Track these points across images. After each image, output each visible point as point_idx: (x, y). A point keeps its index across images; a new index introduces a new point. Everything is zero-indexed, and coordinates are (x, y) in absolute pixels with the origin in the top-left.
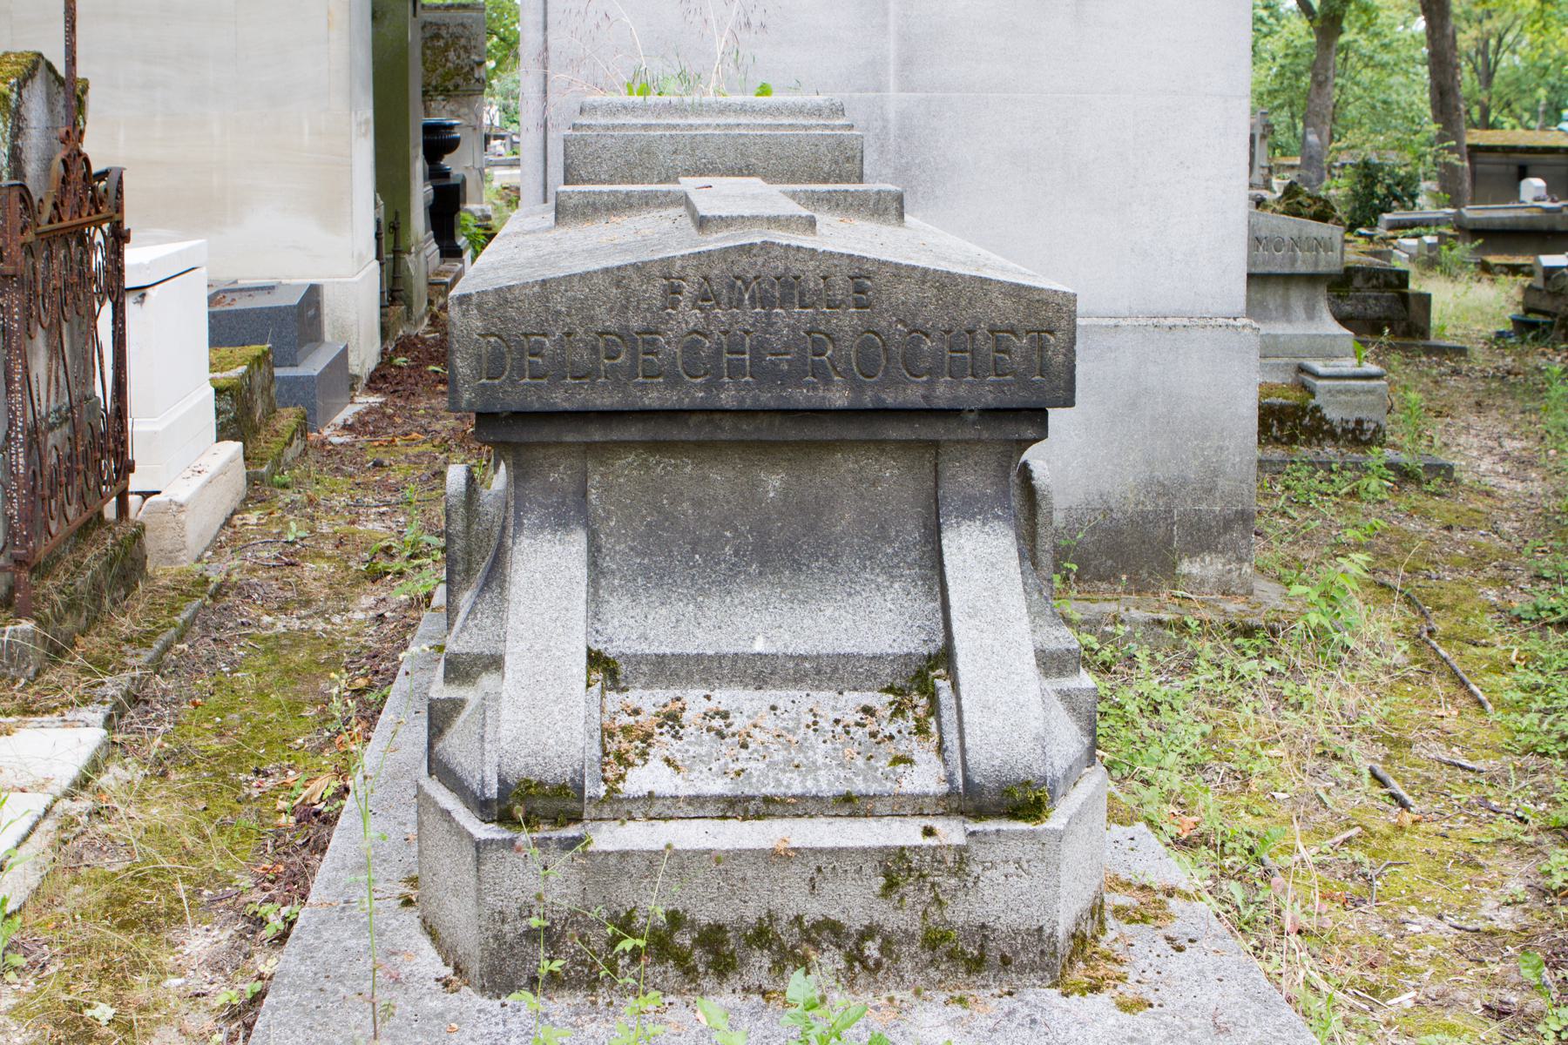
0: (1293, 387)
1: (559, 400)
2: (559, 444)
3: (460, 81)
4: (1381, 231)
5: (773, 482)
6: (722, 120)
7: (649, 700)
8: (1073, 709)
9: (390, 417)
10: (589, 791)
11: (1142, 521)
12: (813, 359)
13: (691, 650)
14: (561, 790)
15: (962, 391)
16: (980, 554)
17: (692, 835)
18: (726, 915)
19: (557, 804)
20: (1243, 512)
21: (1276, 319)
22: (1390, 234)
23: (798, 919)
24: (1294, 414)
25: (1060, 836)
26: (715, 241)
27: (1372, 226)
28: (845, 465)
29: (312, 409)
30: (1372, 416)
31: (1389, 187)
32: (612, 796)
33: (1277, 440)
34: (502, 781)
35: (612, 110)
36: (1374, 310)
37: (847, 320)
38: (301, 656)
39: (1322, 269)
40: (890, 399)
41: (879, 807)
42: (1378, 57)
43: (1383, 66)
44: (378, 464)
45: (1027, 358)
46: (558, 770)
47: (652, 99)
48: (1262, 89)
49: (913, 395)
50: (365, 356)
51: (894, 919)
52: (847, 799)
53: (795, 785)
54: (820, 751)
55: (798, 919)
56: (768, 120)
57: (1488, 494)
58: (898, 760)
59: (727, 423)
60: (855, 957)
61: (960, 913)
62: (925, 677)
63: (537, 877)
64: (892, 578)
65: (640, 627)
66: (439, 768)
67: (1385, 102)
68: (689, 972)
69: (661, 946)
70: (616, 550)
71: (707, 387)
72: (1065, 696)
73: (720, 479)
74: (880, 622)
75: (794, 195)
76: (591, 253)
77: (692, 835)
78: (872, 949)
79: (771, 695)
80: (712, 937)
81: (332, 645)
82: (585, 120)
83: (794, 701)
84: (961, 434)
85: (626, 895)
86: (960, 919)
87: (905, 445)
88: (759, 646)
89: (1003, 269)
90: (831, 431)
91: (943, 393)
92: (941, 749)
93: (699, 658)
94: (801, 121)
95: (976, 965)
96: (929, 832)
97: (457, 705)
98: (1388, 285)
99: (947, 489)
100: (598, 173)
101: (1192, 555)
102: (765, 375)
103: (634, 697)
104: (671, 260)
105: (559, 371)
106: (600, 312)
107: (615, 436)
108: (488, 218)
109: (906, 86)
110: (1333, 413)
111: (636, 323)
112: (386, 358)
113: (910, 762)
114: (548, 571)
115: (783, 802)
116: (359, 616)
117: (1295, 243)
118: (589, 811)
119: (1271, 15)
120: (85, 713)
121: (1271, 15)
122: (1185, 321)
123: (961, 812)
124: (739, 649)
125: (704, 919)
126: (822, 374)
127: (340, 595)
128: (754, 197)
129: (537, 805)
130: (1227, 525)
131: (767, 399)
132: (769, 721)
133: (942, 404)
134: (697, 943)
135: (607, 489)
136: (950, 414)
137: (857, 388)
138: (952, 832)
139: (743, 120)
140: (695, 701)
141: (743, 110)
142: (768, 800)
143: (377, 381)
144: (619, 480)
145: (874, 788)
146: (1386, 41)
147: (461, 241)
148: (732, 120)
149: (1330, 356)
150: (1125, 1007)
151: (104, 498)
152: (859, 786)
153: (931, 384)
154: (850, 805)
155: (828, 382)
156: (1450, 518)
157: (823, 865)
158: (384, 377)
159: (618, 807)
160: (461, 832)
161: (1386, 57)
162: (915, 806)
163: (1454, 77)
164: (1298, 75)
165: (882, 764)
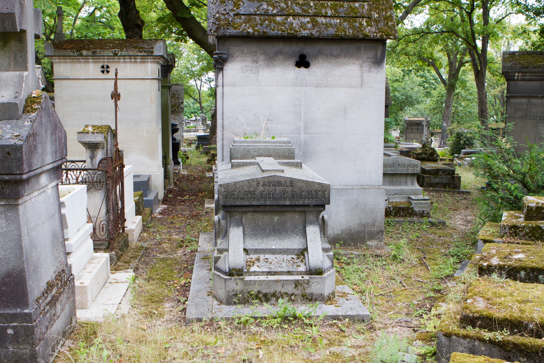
0: (407, 203)
1: (238, 203)
3: (176, 108)
4: (462, 155)
5: (276, 218)
6: (264, 145)
7: (254, 257)
9: (171, 211)
10: (244, 271)
11: (358, 232)
12: (283, 195)
13: (261, 248)
14: (239, 270)
15: (310, 202)
16: (313, 231)
17: (263, 278)
18: (268, 291)
19: (239, 272)
21: (403, 185)
22: (464, 156)
23: (280, 292)
24: (406, 209)
25: (325, 278)
26: (266, 175)
27: (460, 153)
28: (289, 215)
29: (152, 208)
30: (426, 210)
31: (465, 141)
32: (248, 272)
33: (402, 216)
34: (229, 268)
35: (241, 142)
36: (445, 181)
37: (289, 189)
38: (169, 262)
39: (415, 172)
40: (297, 203)
41: (294, 273)
42: (468, 98)
43: (469, 100)
44: (172, 223)
46: (239, 267)
47: (249, 140)
48: (431, 107)
49: (301, 202)
50: (161, 196)
52: (289, 272)
54: (284, 264)
55: (280, 292)
56: (274, 145)
57: (454, 229)
58: (297, 266)
59: (268, 207)
61: (308, 291)
62: (302, 253)
63: (235, 285)
64: (297, 235)
65: (253, 244)
66: (217, 269)
67: (469, 112)
68: (261, 301)
69: (257, 297)
70: (248, 230)
71: (264, 201)
72: (328, 256)
73: (266, 217)
74: (294, 243)
75: (279, 163)
76: (242, 176)
77: (263, 278)
78: (293, 297)
79: (275, 256)
80: (265, 295)
81: (175, 260)
82: (235, 144)
83: (280, 257)
84: (309, 209)
85: (250, 288)
86: (308, 292)
87: (300, 211)
88: (273, 247)
89: (319, 179)
90: (286, 209)
91: (306, 202)
92: (305, 264)
93: (263, 249)
94: (281, 145)
95: (311, 300)
96: (303, 277)
97: (219, 258)
98: (449, 174)
99: (307, 219)
100: (238, 156)
101: (369, 240)
102: (275, 199)
103: (251, 256)
104: (258, 178)
105: (238, 198)
107: (248, 210)
108: (186, 152)
109: (306, 133)
110: (416, 209)
111: (252, 190)
112: (166, 196)
113: (300, 266)
114: (236, 234)
115: (278, 272)
116: (179, 254)
117: (409, 165)
118: (244, 274)
119: (436, 82)
120: (129, 270)
121: (436, 82)
123: (309, 274)
124: (270, 247)
125: (264, 292)
126: (285, 199)
127: (174, 251)
128: (272, 164)
129: (235, 273)
131: (275, 203)
132: (275, 260)
133: (306, 204)
134: (263, 296)
135: (246, 219)
136: (308, 206)
138: (307, 277)
139: (269, 144)
140: (262, 257)
141: (269, 142)
142: (275, 272)
143: (165, 201)
144: (248, 218)
145: (293, 270)
146: (471, 92)
147: (180, 160)
148: (266, 144)
149: (417, 195)
150: (336, 306)
151: (119, 229)
152: (291, 270)
153: (304, 200)
154: (289, 273)
155: (286, 200)
156: (441, 234)
158: (166, 200)
159: (249, 273)
160: (222, 278)
161: (470, 97)
162: (300, 273)
163: (486, 107)
164: (442, 103)
165: (295, 267)
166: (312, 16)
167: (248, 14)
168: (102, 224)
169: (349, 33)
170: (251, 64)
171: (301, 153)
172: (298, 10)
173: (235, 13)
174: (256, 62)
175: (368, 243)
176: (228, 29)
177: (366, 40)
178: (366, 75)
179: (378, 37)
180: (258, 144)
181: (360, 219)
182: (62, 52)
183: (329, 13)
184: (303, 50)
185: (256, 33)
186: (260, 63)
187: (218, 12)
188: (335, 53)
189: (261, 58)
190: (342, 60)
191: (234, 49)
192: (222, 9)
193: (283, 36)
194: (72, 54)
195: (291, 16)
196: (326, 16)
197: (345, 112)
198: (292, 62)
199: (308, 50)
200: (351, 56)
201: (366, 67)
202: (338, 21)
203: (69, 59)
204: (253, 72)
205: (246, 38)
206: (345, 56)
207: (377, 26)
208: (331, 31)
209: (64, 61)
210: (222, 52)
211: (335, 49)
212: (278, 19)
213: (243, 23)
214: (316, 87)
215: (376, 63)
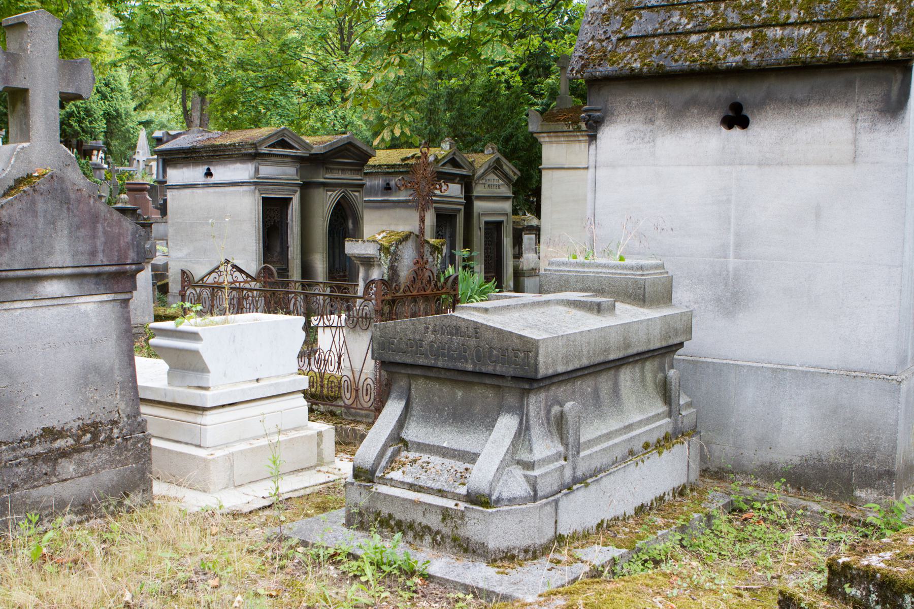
2: (485, 384)
5: (460, 393)
8: (528, 482)
11: (836, 467)
15: (504, 369)
18: (403, 518)
20: (889, 471)
23: (420, 523)
28: (479, 391)
37: (473, 342)
40: (484, 370)
45: (523, 360)
49: (489, 369)
51: (446, 530)
53: (430, 484)
55: (420, 523)
60: (434, 539)
61: (462, 532)
73: (445, 390)
88: (445, 445)
91: (499, 369)
93: (429, 445)
94: (625, 272)
95: (466, 550)
101: (861, 488)
102: (451, 358)
105: (399, 350)
106: (408, 332)
109: (738, 256)
111: (417, 337)
122: (864, 374)
125: (397, 518)
130: (880, 476)
131: (450, 365)
134: (396, 524)
135: (417, 389)
136: (501, 377)
137: (475, 364)
138: (462, 506)
139: (604, 270)
142: (420, 487)
144: (419, 387)
148: (600, 270)
152: (446, 488)
153: (495, 366)
154: (441, 493)
155: (467, 361)
157: (428, 508)
162: (457, 497)
166: (759, 26)
167: (642, 37)
168: (366, 383)
169: (823, 52)
170: (642, 127)
171: (728, 294)
172: (733, 17)
173: (621, 36)
174: (652, 121)
175: (858, 493)
176: (600, 65)
177: (859, 65)
178: (865, 139)
179: (885, 55)
180: (586, 270)
181: (841, 440)
182: (553, 126)
183: (794, 16)
184: (732, 94)
185: (645, 69)
186: (657, 123)
187: (593, 38)
188: (799, 96)
189: (661, 114)
190: (814, 109)
191: (616, 99)
192: (601, 32)
193: (692, 70)
194: (565, 128)
195: (717, 31)
196: (784, 25)
197: (818, 216)
198: (716, 118)
199: (745, 93)
200: (833, 100)
201: (865, 121)
202: (808, 31)
203: (564, 136)
204: (647, 140)
205: (632, 80)
206: (821, 102)
207: (889, 32)
208: (787, 52)
209: (556, 139)
210: (593, 107)
211: (799, 87)
212: (694, 38)
213: (629, 52)
214: (760, 165)
215: (889, 112)
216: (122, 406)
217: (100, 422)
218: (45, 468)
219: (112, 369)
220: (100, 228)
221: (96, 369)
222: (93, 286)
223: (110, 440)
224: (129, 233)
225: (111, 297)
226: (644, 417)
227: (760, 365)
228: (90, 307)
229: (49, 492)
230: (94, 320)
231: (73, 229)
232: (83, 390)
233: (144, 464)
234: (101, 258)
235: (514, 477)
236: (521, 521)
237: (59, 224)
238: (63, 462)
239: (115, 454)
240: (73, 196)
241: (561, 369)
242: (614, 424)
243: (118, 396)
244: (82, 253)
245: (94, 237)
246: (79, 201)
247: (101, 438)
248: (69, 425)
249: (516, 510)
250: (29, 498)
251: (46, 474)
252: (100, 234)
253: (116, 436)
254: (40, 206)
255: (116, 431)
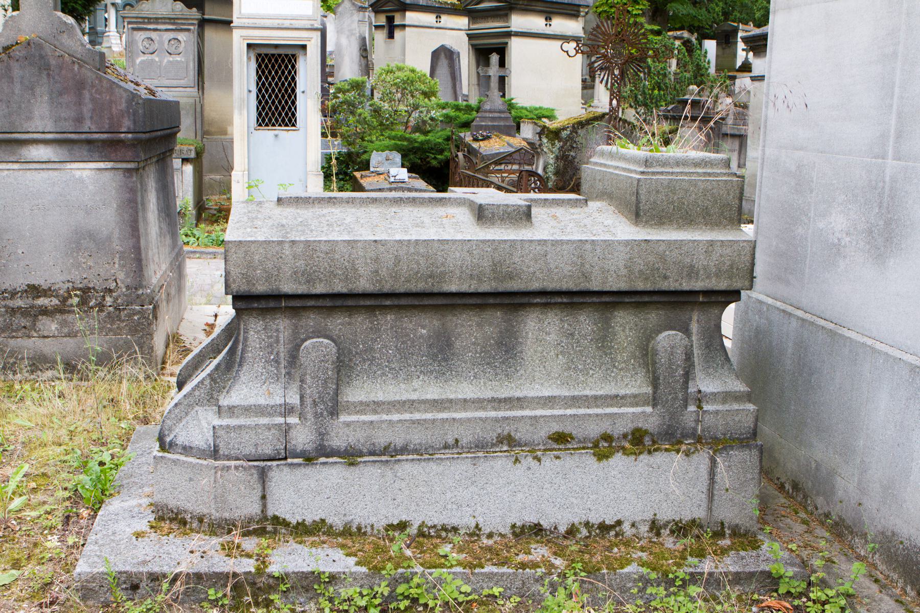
171: (881, 223)
216: (121, 276)
217: (94, 288)
218: (24, 322)
219: (109, 238)
220: (87, 94)
221: (91, 236)
222: (85, 153)
223: (101, 306)
224: (123, 100)
225: (109, 165)
226: (565, 392)
227: (897, 354)
228: (86, 173)
229: (29, 345)
230: (91, 187)
231: (54, 95)
232: (75, 255)
233: (142, 337)
234: (87, 125)
235: (199, 420)
236: (191, 480)
237: (38, 90)
238: (43, 321)
239: (105, 322)
240: (53, 62)
241: (288, 288)
242: (432, 390)
243: (117, 266)
244: (65, 119)
245: (80, 103)
246: (61, 68)
247: (91, 304)
248: (57, 286)
249: (184, 462)
250: (7, 346)
251: (25, 327)
252: (87, 100)
253: (109, 304)
254: (17, 72)
255: (108, 299)
